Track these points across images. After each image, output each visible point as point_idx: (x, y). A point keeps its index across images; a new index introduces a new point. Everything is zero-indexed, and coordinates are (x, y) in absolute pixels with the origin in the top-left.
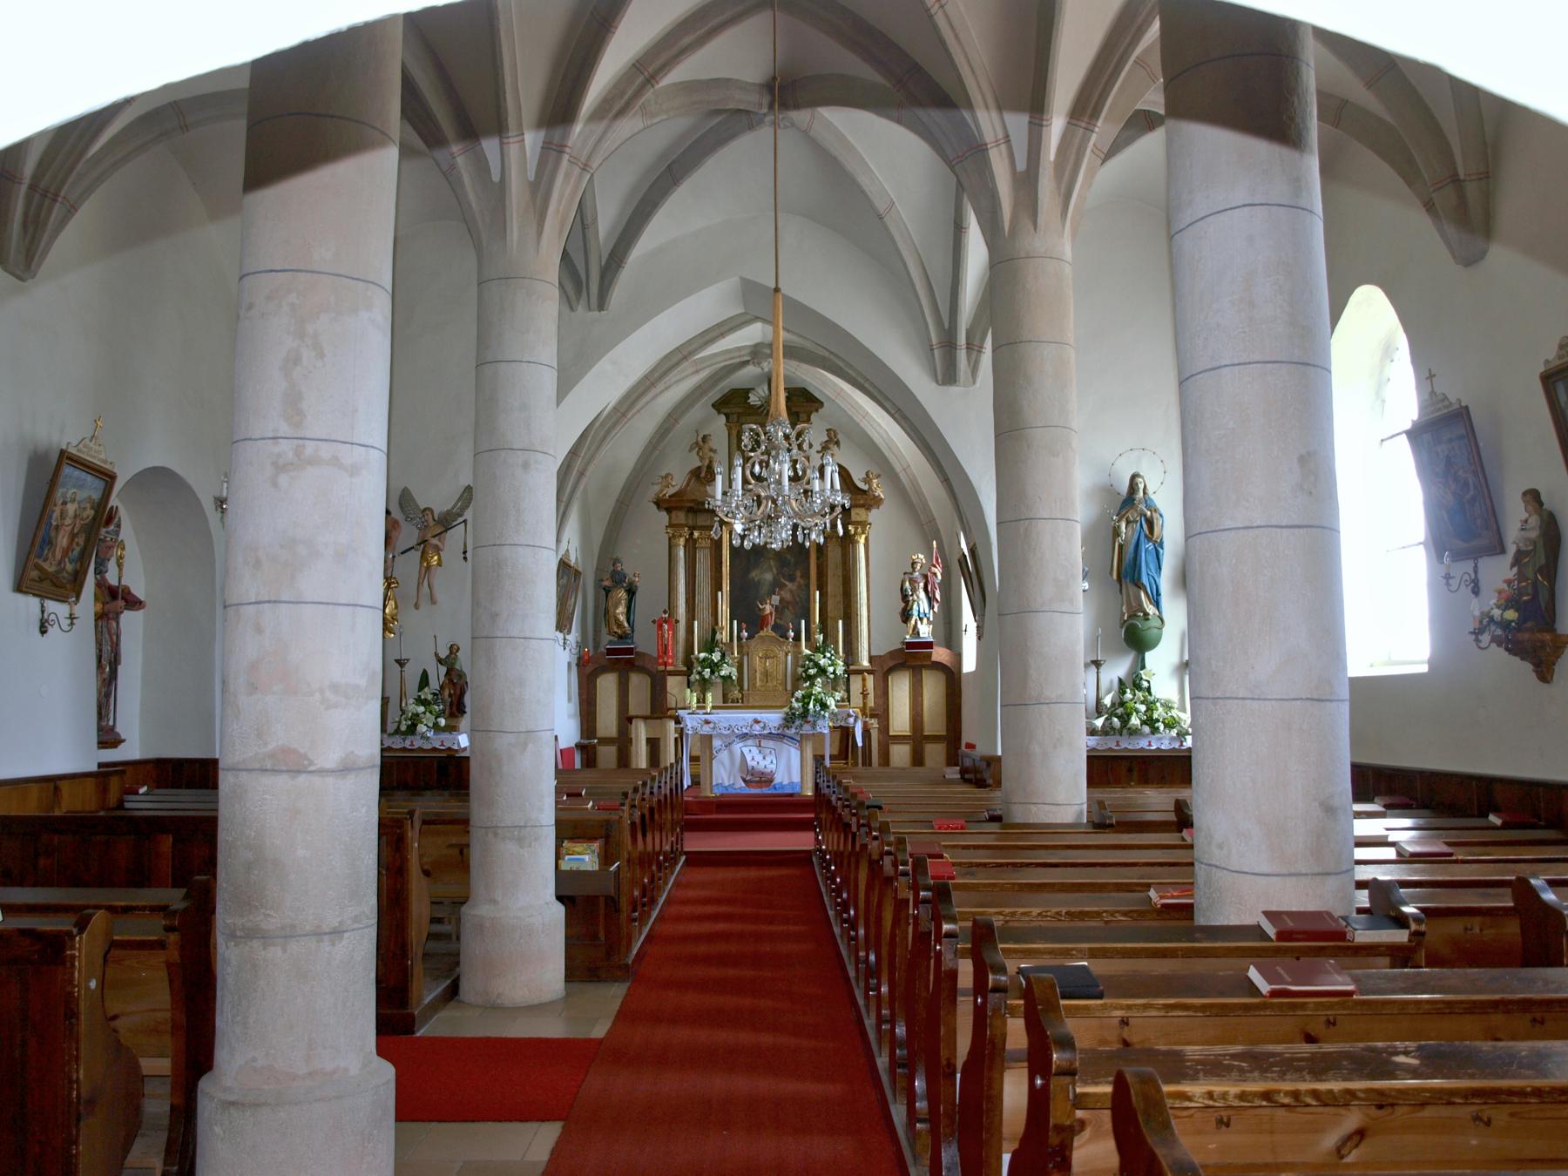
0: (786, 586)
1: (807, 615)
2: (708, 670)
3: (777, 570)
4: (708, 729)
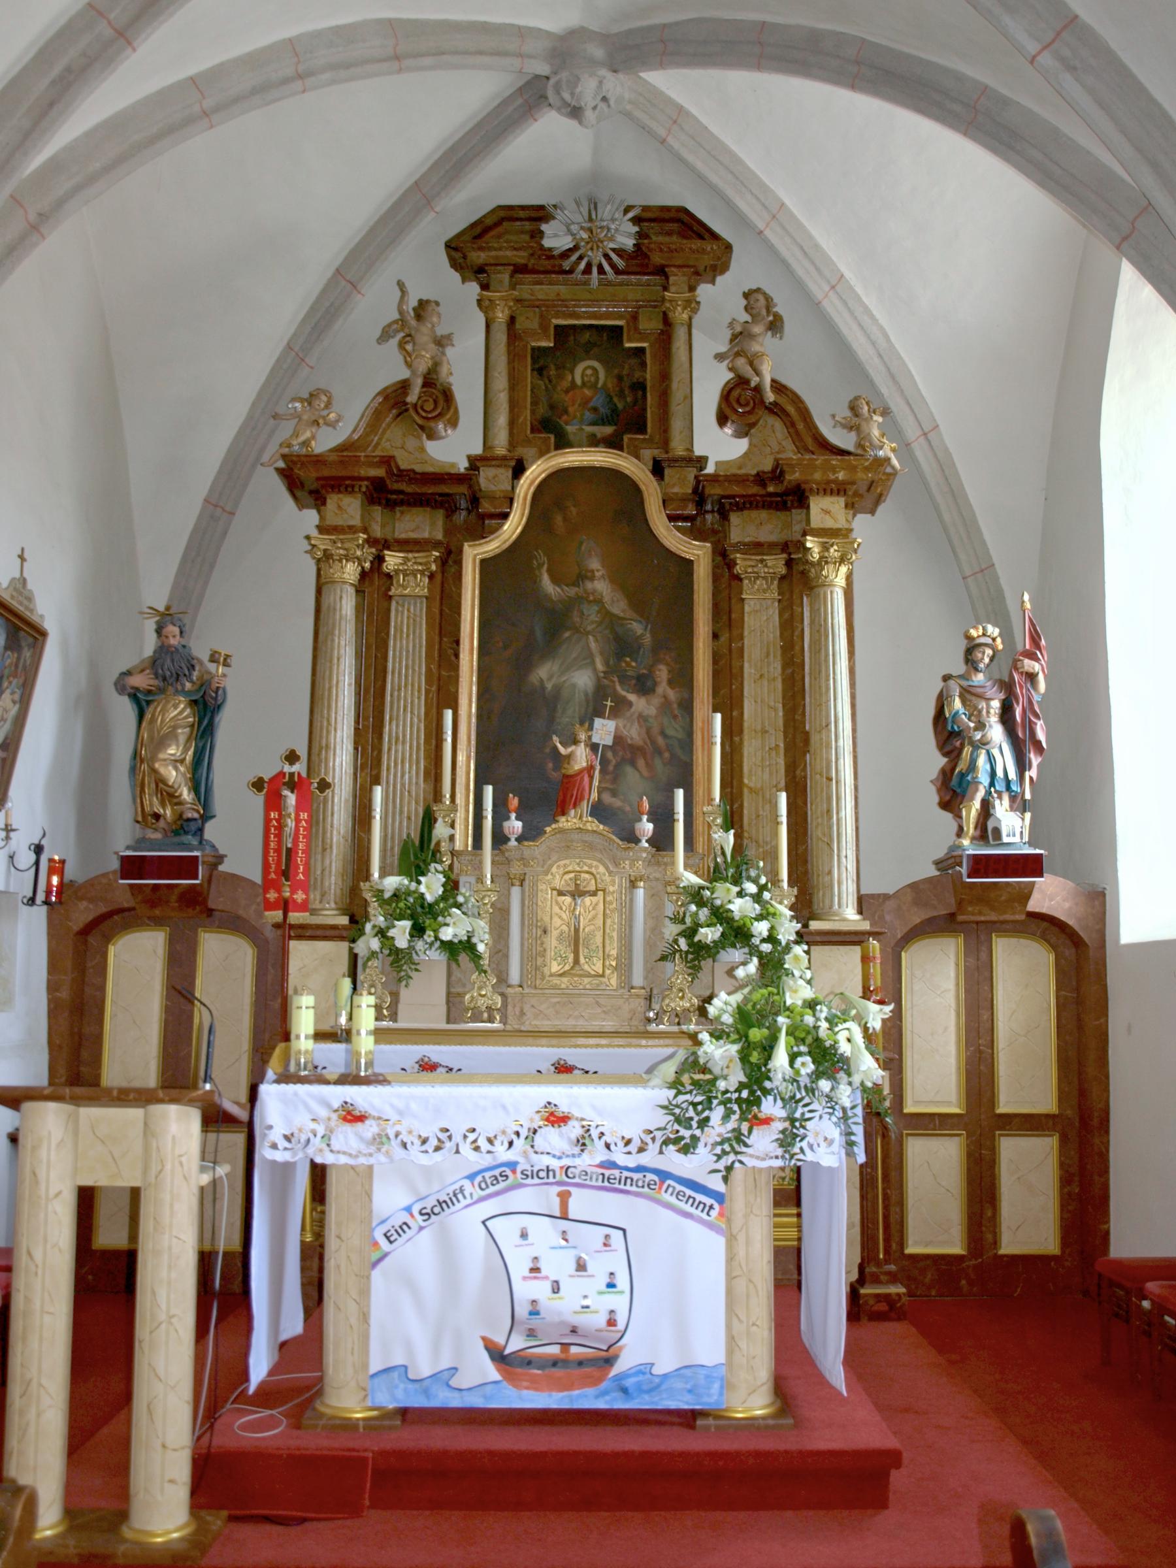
0: (630, 704)
1: (685, 776)
2: (406, 924)
3: (607, 663)
4: (354, 1144)
